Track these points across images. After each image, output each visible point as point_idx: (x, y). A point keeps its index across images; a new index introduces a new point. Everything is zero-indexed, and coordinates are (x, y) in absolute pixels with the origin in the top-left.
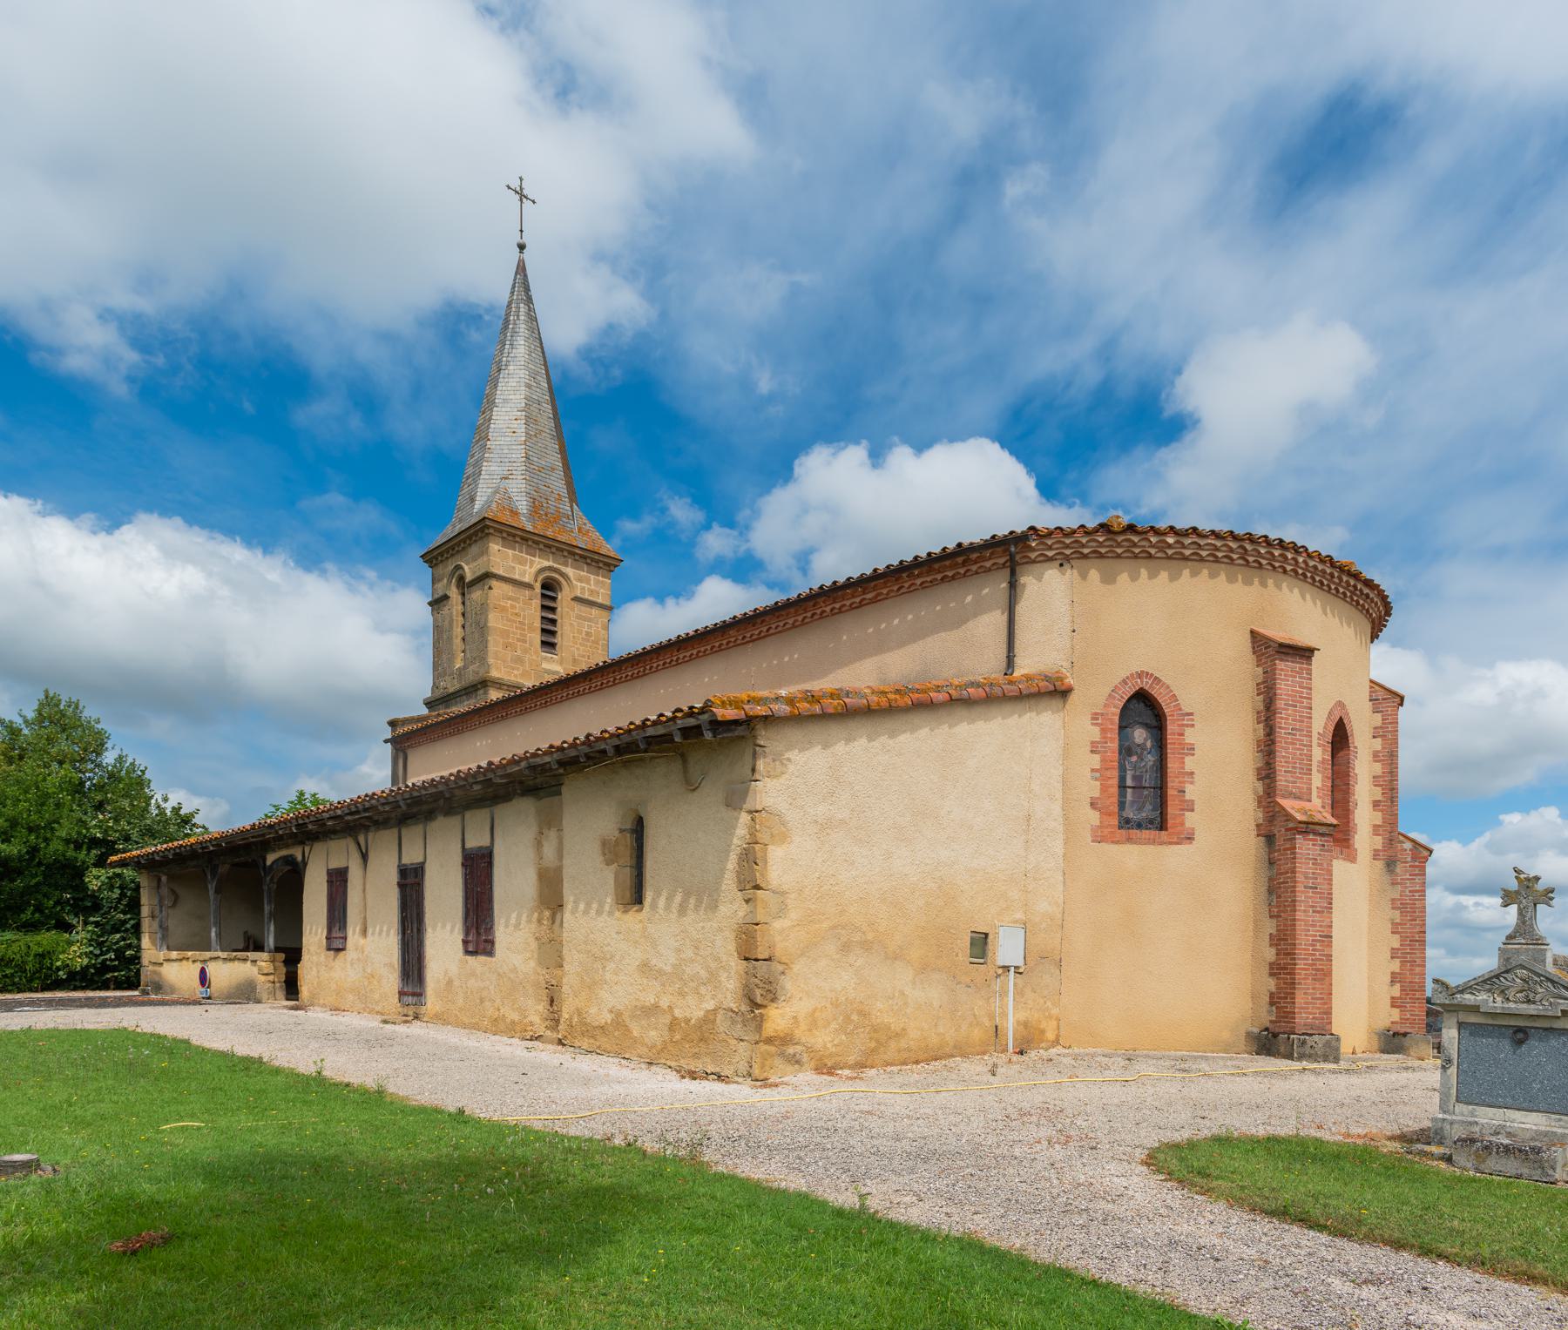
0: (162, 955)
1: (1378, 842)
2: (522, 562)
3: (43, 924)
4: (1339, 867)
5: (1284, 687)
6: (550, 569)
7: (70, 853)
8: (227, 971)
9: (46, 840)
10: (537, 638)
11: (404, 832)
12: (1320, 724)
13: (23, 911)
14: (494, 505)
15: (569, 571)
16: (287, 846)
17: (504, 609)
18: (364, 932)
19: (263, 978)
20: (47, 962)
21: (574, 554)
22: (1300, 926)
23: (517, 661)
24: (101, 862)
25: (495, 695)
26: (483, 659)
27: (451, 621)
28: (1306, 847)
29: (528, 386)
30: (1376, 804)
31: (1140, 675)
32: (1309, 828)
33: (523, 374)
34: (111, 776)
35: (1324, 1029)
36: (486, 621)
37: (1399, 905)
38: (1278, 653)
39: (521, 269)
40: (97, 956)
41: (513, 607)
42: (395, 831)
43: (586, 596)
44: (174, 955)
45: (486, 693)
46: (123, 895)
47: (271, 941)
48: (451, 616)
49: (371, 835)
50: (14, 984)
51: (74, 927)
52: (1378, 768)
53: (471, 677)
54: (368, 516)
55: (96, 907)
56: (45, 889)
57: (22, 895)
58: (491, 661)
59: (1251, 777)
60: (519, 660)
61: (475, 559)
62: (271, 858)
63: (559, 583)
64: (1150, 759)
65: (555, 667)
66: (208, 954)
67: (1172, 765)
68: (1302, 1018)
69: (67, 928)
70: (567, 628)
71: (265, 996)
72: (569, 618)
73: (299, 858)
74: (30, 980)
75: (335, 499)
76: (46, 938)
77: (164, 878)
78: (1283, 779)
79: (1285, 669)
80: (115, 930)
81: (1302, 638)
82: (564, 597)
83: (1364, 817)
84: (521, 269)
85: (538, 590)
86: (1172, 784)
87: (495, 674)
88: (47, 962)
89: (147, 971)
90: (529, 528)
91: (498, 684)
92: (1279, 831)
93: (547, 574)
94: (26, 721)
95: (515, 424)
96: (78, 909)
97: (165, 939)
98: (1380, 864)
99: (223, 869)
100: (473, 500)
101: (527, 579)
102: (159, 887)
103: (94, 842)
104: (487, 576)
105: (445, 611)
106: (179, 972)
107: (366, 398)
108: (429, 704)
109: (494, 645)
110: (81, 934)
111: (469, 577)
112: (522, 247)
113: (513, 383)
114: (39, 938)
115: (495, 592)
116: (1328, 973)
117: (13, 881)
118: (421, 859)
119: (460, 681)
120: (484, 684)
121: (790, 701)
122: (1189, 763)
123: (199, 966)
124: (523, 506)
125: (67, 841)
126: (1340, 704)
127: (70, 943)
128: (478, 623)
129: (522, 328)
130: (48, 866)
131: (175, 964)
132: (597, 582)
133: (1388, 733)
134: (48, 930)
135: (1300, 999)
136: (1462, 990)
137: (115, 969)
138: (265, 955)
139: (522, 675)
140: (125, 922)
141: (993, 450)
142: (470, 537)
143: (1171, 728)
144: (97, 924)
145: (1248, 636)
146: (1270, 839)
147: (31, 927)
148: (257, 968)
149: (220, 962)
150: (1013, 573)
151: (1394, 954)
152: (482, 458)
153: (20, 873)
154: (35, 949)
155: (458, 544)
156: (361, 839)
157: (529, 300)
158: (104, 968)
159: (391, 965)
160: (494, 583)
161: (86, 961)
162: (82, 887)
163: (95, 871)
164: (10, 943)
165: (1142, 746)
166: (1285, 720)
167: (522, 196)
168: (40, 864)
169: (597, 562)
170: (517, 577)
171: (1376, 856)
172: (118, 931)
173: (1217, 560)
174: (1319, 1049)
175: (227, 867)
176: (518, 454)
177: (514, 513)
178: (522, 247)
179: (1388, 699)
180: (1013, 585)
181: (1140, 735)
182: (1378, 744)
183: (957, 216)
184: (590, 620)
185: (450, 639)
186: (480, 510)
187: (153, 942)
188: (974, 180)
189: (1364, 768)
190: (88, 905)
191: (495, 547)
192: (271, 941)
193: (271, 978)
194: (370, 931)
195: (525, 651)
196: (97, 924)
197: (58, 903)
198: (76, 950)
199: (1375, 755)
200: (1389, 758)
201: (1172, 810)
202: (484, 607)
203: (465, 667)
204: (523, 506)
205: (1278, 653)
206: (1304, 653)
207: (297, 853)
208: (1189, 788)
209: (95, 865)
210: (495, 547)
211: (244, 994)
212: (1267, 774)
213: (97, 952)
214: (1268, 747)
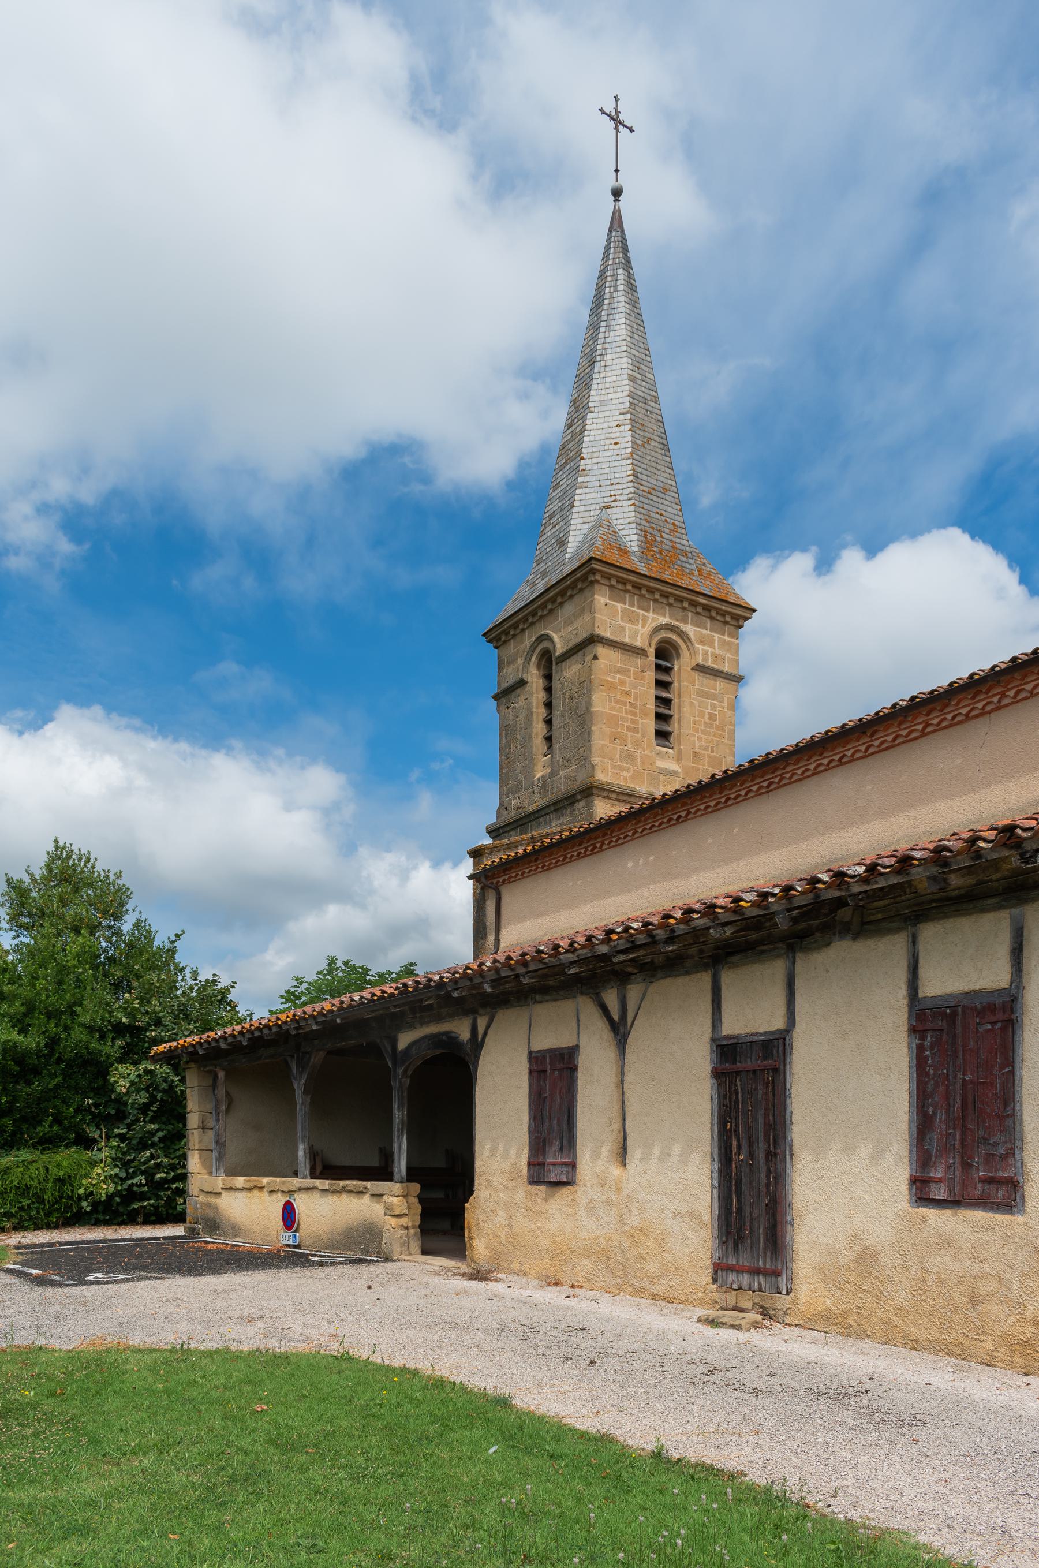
0: (220, 1181)
2: (632, 619)
3: (62, 1139)
6: (667, 627)
7: (94, 1045)
8: (326, 1209)
9: (66, 1028)
11: (727, 978)
13: (40, 1123)
14: (599, 542)
15: (689, 629)
16: (439, 1019)
17: (611, 687)
18: (622, 1154)
19: (393, 1222)
20: (68, 1189)
21: (694, 604)
23: (631, 763)
24: (129, 1055)
25: (603, 809)
26: (584, 759)
29: (632, 379)
33: (624, 362)
34: (130, 945)
36: (589, 704)
39: (616, 222)
40: (123, 1180)
41: (622, 683)
42: (705, 979)
43: (709, 663)
44: (240, 1181)
45: (590, 805)
46: (153, 1099)
47: (401, 1165)
49: (633, 992)
50: (31, 1218)
51: (94, 1141)
53: (562, 786)
54: (263, 684)
55: (121, 1116)
56: (64, 1093)
57: (39, 1102)
58: (596, 760)
60: (629, 757)
61: (569, 623)
62: (405, 1040)
63: (676, 648)
65: (665, 772)
66: (296, 1182)
69: (88, 1143)
70: (686, 709)
71: (396, 1250)
72: (690, 693)
73: (465, 1035)
74: (48, 1214)
75: (229, 668)
76: (66, 1157)
77: (221, 1075)
80: (143, 1146)
82: (682, 666)
84: (616, 222)
85: (652, 658)
87: (601, 777)
88: (68, 1189)
89: (196, 1200)
90: (644, 571)
91: (608, 792)
93: (663, 634)
94: (34, 880)
96: (98, 1120)
97: (221, 1158)
99: (317, 1058)
100: (562, 543)
101: (638, 643)
102: (214, 1086)
103: (119, 1030)
104: (592, 640)
105: (521, 702)
106: (249, 1208)
107: (259, 556)
108: (494, 832)
109: (600, 738)
110: (105, 1152)
111: (560, 648)
112: (617, 193)
114: (58, 1157)
117: (29, 1083)
118: (778, 1023)
119: (543, 795)
120: (589, 791)
123: (280, 1200)
124: (632, 541)
125: (91, 1029)
127: (93, 1164)
128: (574, 711)
129: (621, 300)
130: (70, 1064)
131: (241, 1195)
132: (723, 643)
134: (67, 1147)
137: (142, 1197)
138: (396, 1187)
139: (633, 778)
140: (152, 1134)
141: (956, 534)
142: (562, 593)
144: (122, 1138)
147: (48, 1143)
148: (385, 1206)
149: (316, 1195)
152: (575, 485)
153: (36, 1072)
154: (56, 1172)
155: (543, 606)
156: (611, 998)
157: (628, 265)
158: (131, 1195)
159: (693, 1216)
160: (601, 650)
161: (112, 1188)
162: (105, 1089)
163: (121, 1068)
164: (27, 1164)
167: (617, 121)
168: (59, 1060)
169: (723, 614)
170: (627, 640)
172: (145, 1147)
175: (322, 1054)
176: (625, 470)
177: (624, 552)
178: (617, 193)
183: (919, 245)
184: (713, 697)
185: (527, 740)
187: (204, 1161)
188: (944, 198)
190: (113, 1113)
191: (601, 598)
192: (401, 1165)
193: (404, 1221)
194: (635, 1153)
195: (637, 744)
196: (122, 1138)
197: (78, 1110)
198: (99, 1174)
202: (586, 686)
203: (552, 774)
204: (632, 541)
207: (462, 1030)
209: (121, 1060)
210: (601, 598)
211: (362, 1247)
213: (123, 1175)
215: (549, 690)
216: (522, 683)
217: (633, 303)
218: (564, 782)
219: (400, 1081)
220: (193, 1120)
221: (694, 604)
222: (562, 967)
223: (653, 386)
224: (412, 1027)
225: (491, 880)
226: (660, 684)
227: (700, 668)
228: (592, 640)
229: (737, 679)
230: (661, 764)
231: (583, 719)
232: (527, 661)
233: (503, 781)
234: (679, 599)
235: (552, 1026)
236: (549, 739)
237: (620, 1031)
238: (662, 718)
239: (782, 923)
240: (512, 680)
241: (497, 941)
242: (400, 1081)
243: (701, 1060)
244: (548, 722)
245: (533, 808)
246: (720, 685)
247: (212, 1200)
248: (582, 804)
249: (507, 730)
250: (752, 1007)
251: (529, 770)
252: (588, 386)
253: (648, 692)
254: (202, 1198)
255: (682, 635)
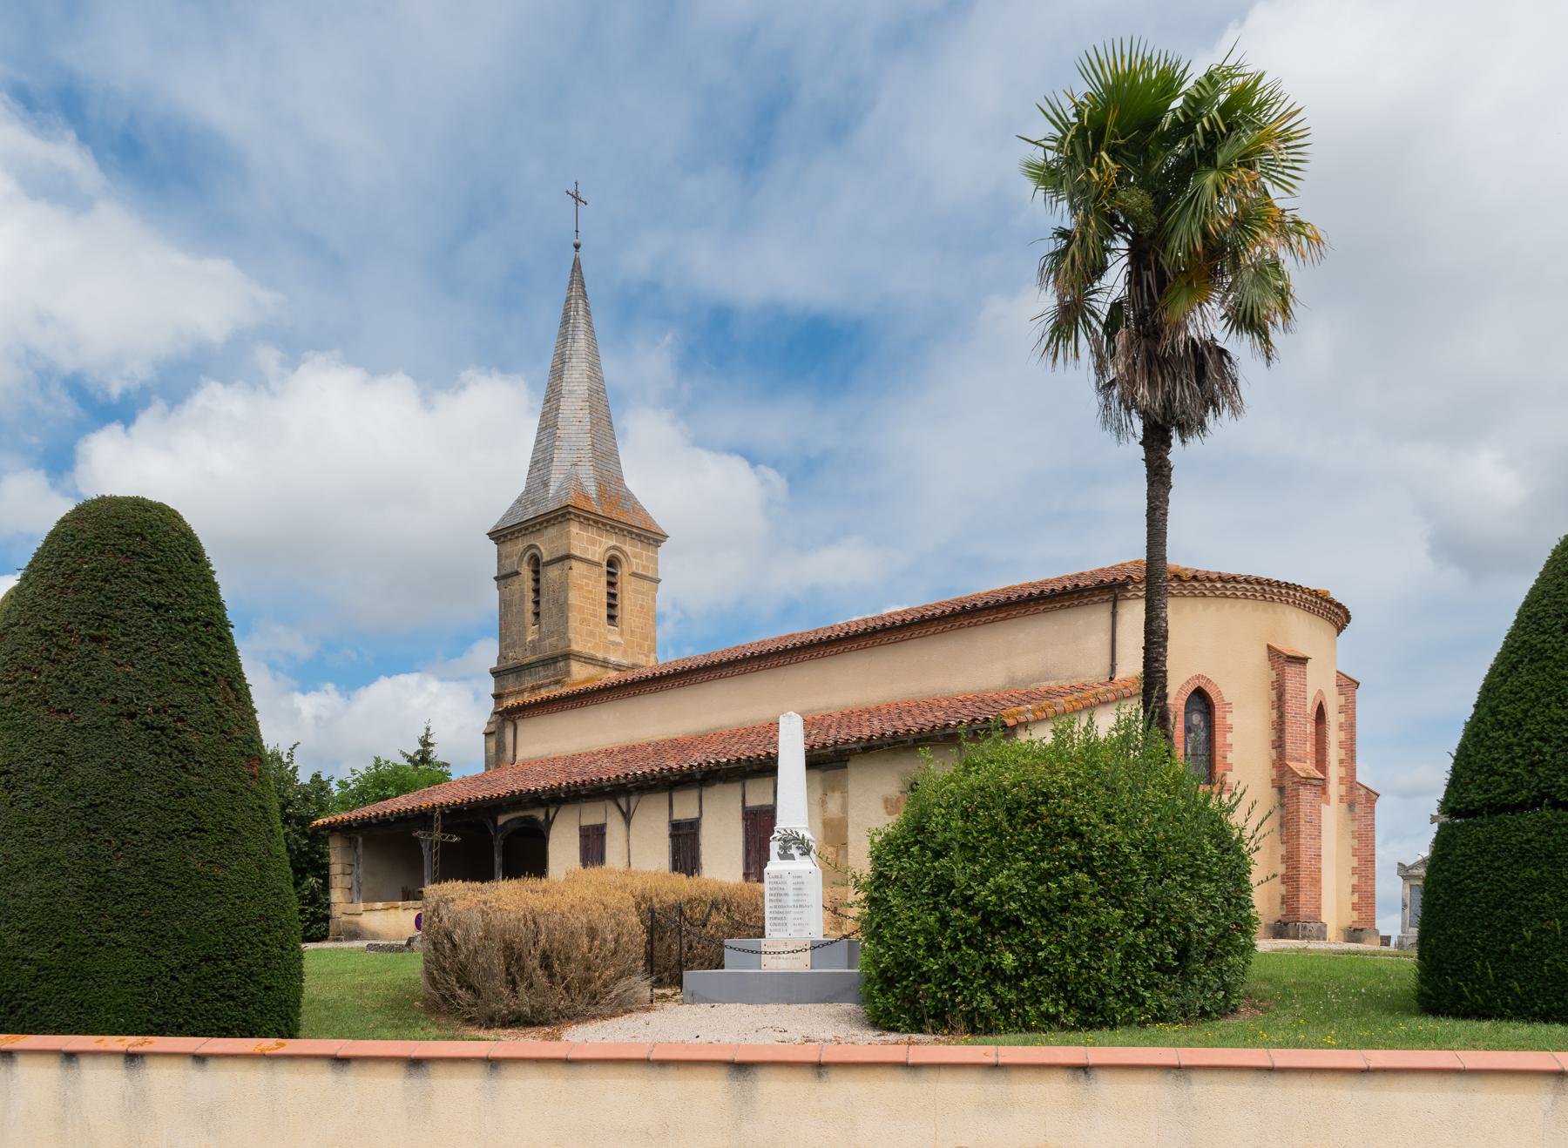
1: (1343, 790)
4: (1324, 806)
5: (1290, 685)
6: (614, 548)
10: (604, 611)
12: (1311, 709)
15: (627, 548)
16: (525, 808)
17: (580, 588)
21: (630, 533)
22: (1302, 848)
25: (580, 675)
27: (522, 597)
28: (1306, 795)
29: (590, 378)
30: (1341, 762)
31: (1198, 677)
32: (1306, 781)
33: (584, 366)
35: (1317, 920)
36: (566, 598)
37: (1357, 835)
38: (1285, 662)
39: (576, 266)
48: (522, 592)
52: (1342, 735)
58: (571, 635)
59: (1268, 746)
60: (591, 634)
62: (502, 820)
64: (1203, 735)
67: (1218, 739)
68: (1304, 911)
70: (626, 602)
73: (541, 817)
78: (1290, 748)
79: (1291, 670)
81: (1301, 651)
82: (623, 572)
83: (1335, 771)
84: (576, 266)
85: (605, 568)
86: (1219, 752)
87: (575, 647)
92: (1288, 784)
93: (612, 552)
95: (580, 414)
98: (1344, 806)
104: (568, 557)
105: (516, 587)
112: (577, 247)
113: (576, 374)
115: (575, 572)
116: (1319, 881)
118: (696, 815)
121: (1033, 712)
122: (1230, 738)
124: (592, 491)
126: (1320, 692)
128: (556, 601)
133: (1348, 709)
135: (1302, 898)
136: (1412, 867)
142: (548, 521)
143: (1218, 713)
145: (1264, 652)
146: (1281, 790)
150: (1114, 606)
151: (1354, 871)
156: (623, 802)
160: (574, 563)
165: (1197, 726)
166: (1291, 707)
167: (577, 199)
171: (1341, 800)
173: (1247, 598)
174: (1314, 932)
176: (586, 441)
177: (587, 498)
178: (577, 247)
179: (1348, 685)
180: (1114, 615)
181: (1196, 718)
182: (1342, 718)
185: (521, 613)
186: (557, 496)
189: (1334, 736)
195: (596, 625)
199: (1341, 726)
200: (1350, 727)
201: (1219, 771)
202: (564, 586)
203: (540, 640)
204: (592, 491)
205: (1285, 662)
206: (1303, 661)
207: (540, 815)
208: (1229, 755)
212: (1279, 745)
214: (1280, 726)
215: (537, 581)
216: (517, 573)
217: (589, 324)
218: (549, 647)
219: (498, 843)
220: (336, 868)
221: (630, 533)
222: (602, 788)
223: (601, 381)
224: (506, 812)
225: (507, 716)
226: (611, 584)
227: (634, 575)
228: (568, 557)
229: (658, 581)
230: (611, 638)
231: (563, 608)
232: (521, 559)
233: (502, 638)
234: (622, 530)
235: (592, 815)
236: (537, 614)
237: (627, 817)
238: (611, 606)
239: (698, 776)
240: (508, 570)
241: (515, 756)
242: (498, 843)
243: (664, 830)
244: (537, 603)
245: (526, 661)
246: (647, 584)
247: (354, 918)
248: (562, 664)
249: (505, 604)
250: (685, 808)
251: (522, 633)
252: (561, 377)
253: (603, 589)
254: (344, 918)
255: (622, 552)
